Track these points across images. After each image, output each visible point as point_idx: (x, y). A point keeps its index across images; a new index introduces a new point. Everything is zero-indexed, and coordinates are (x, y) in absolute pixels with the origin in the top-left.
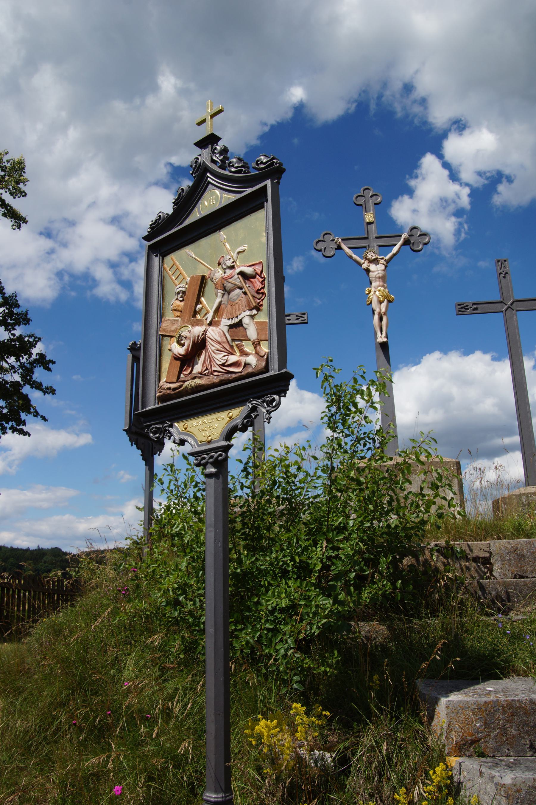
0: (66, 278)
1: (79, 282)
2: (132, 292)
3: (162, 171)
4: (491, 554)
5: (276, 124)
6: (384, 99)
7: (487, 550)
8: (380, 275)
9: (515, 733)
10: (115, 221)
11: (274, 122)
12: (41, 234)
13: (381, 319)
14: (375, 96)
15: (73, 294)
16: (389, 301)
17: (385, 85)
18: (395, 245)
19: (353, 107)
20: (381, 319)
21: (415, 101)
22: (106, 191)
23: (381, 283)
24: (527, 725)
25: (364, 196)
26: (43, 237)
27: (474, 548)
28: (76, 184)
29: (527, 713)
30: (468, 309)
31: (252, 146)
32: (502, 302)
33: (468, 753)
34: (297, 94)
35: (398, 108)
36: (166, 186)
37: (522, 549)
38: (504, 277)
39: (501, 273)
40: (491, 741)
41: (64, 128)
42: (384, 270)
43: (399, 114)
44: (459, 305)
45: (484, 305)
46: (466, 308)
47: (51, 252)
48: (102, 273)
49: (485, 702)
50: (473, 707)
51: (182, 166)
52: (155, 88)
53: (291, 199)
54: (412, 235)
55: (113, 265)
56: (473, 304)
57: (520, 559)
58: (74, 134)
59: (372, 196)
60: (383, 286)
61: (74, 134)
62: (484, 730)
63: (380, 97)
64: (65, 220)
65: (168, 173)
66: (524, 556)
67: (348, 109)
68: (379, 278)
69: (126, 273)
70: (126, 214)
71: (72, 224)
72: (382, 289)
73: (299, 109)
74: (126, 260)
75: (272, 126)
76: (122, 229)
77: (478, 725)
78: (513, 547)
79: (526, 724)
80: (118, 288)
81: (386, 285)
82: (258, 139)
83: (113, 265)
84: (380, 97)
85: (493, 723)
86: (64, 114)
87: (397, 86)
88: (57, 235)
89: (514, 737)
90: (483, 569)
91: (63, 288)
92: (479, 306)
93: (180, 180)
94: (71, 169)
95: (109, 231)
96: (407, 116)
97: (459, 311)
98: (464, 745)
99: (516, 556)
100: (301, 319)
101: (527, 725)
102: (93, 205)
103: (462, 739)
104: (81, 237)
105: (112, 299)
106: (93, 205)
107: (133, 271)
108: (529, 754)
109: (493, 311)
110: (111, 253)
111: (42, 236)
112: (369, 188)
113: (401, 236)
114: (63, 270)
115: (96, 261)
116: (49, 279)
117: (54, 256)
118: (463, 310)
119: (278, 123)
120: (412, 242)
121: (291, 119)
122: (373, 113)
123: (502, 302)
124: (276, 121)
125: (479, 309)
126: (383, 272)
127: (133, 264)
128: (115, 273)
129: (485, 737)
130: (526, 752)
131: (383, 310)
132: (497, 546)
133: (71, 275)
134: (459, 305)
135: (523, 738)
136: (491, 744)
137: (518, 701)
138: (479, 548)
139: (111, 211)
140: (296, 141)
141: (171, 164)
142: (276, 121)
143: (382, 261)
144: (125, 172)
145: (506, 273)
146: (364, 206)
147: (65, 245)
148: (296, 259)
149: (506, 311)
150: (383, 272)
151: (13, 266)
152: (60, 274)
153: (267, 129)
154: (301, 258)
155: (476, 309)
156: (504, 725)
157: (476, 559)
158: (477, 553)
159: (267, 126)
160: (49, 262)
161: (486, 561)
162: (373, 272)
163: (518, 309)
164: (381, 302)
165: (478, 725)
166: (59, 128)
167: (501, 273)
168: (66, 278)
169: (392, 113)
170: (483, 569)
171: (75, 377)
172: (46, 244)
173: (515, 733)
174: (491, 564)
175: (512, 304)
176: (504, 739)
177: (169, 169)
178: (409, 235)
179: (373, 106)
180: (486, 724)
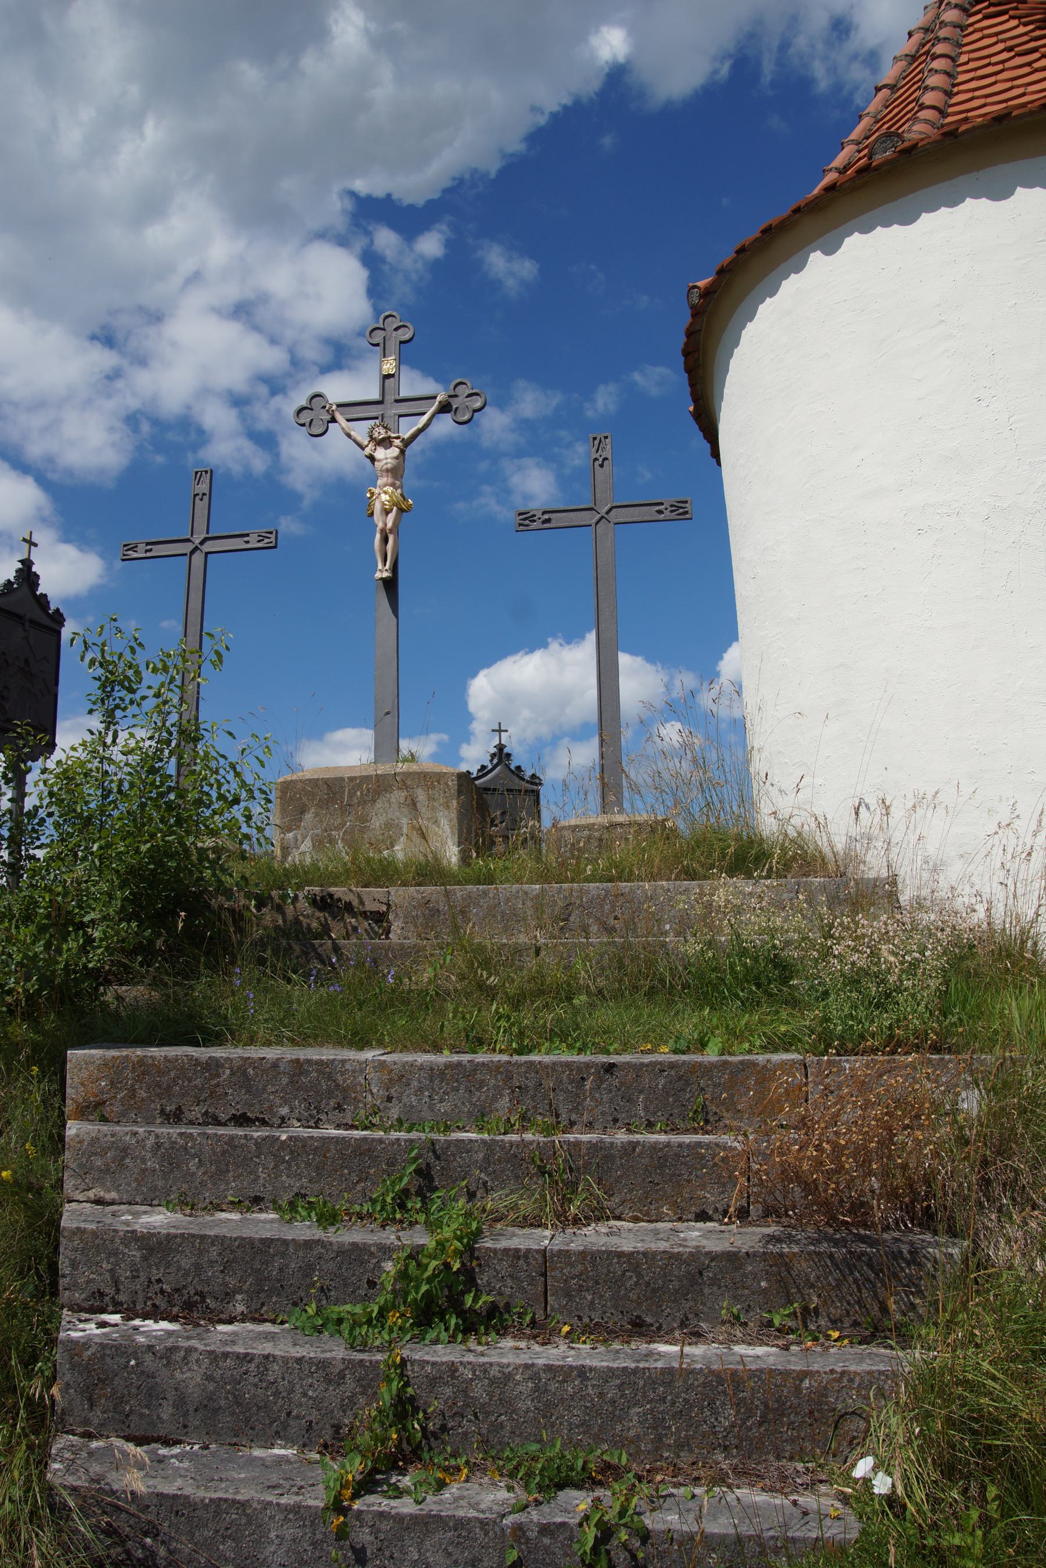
0: (145, 427)
1: (170, 436)
2: (277, 455)
3: (334, 209)
4: (389, 905)
5: (560, 109)
6: (791, 51)
7: (385, 900)
8: (389, 466)
9: (145, 1095)
10: (242, 312)
11: (555, 108)
12: (93, 338)
13: (385, 540)
14: (775, 44)
15: (160, 459)
16: (401, 510)
17: (794, 22)
18: (423, 414)
19: (725, 69)
20: (385, 540)
21: (854, 57)
22: (221, 250)
23: (390, 480)
24: (160, 1087)
25: (384, 329)
26: (98, 345)
27: (364, 897)
28: (162, 236)
29: (160, 1073)
30: (534, 521)
31: (512, 155)
32: (591, 509)
33: (91, 1117)
34: (612, 43)
35: (819, 71)
36: (342, 242)
37: (437, 902)
38: (601, 466)
39: (596, 459)
40: (117, 1104)
41: (136, 122)
42: (397, 458)
43: (823, 84)
44: (520, 514)
45: (563, 514)
46: (532, 518)
47: (114, 375)
48: (217, 418)
49: (113, 1057)
50: (98, 1062)
51: (374, 196)
52: (318, 33)
53: (593, 267)
54: (456, 396)
55: (238, 402)
56: (544, 513)
57: (432, 916)
58: (154, 132)
59: (396, 329)
60: (393, 485)
61: (154, 132)
62: (110, 1090)
63: (784, 46)
64: (141, 309)
65: (344, 211)
66: (438, 911)
67: (716, 72)
68: (387, 471)
69: (263, 417)
70: (264, 298)
71: (156, 317)
72: (390, 489)
73: (617, 76)
74: (263, 390)
75: (554, 116)
76: (256, 328)
77: (103, 1084)
78: (423, 898)
79: (158, 1085)
80: (247, 446)
81: (398, 483)
82: (521, 141)
83: (238, 402)
84: (784, 46)
85: (121, 1082)
86: (134, 91)
87: (818, 21)
88: (126, 340)
89: (143, 1099)
90: (376, 929)
91: (140, 448)
92: (553, 516)
93: (370, 228)
94: (151, 205)
95: (230, 331)
96: (837, 87)
97: (520, 525)
98: (88, 1107)
99: (427, 911)
100: (266, 540)
101: (160, 1087)
102: (195, 278)
103: (85, 1100)
104: (174, 344)
105: (237, 469)
106: (195, 278)
107: (279, 411)
108: (159, 1121)
109: (576, 524)
110: (234, 376)
111: (95, 342)
112: (394, 314)
113: (435, 398)
114: (138, 411)
115: (204, 392)
116: (111, 429)
117: (120, 384)
118: (527, 522)
119: (565, 108)
120: (454, 407)
121: (596, 94)
122: (769, 78)
123: (591, 509)
124: (559, 105)
125: (553, 521)
126: (394, 462)
127: (278, 399)
128: (243, 418)
129: (111, 1099)
130: (155, 1118)
131: (390, 525)
132: (399, 894)
133: (156, 422)
134: (520, 514)
135: (154, 1101)
136: (117, 1108)
137: (151, 1057)
138: (373, 897)
139: (232, 292)
140: (607, 141)
141: (352, 194)
142: (559, 105)
143: (397, 442)
144: (258, 212)
145: (606, 459)
146: (382, 345)
147: (142, 361)
148: (601, 388)
149: (597, 524)
150: (394, 462)
151: (39, 404)
152: (132, 420)
153: (542, 120)
154: (612, 388)
155: (548, 521)
156: (133, 1086)
157: (365, 915)
158: (370, 906)
159: (542, 113)
160: (109, 396)
161: (379, 918)
162: (379, 461)
163: (617, 520)
164: (387, 512)
165: (103, 1084)
166: (119, 119)
167: (596, 459)
168: (145, 427)
169: (806, 83)
170: (376, 929)
171: (165, 624)
172: (103, 359)
173: (145, 1095)
174: (388, 921)
175: (608, 513)
176: (132, 1102)
177: (349, 205)
178: (450, 396)
179: (768, 68)
180: (112, 1083)
